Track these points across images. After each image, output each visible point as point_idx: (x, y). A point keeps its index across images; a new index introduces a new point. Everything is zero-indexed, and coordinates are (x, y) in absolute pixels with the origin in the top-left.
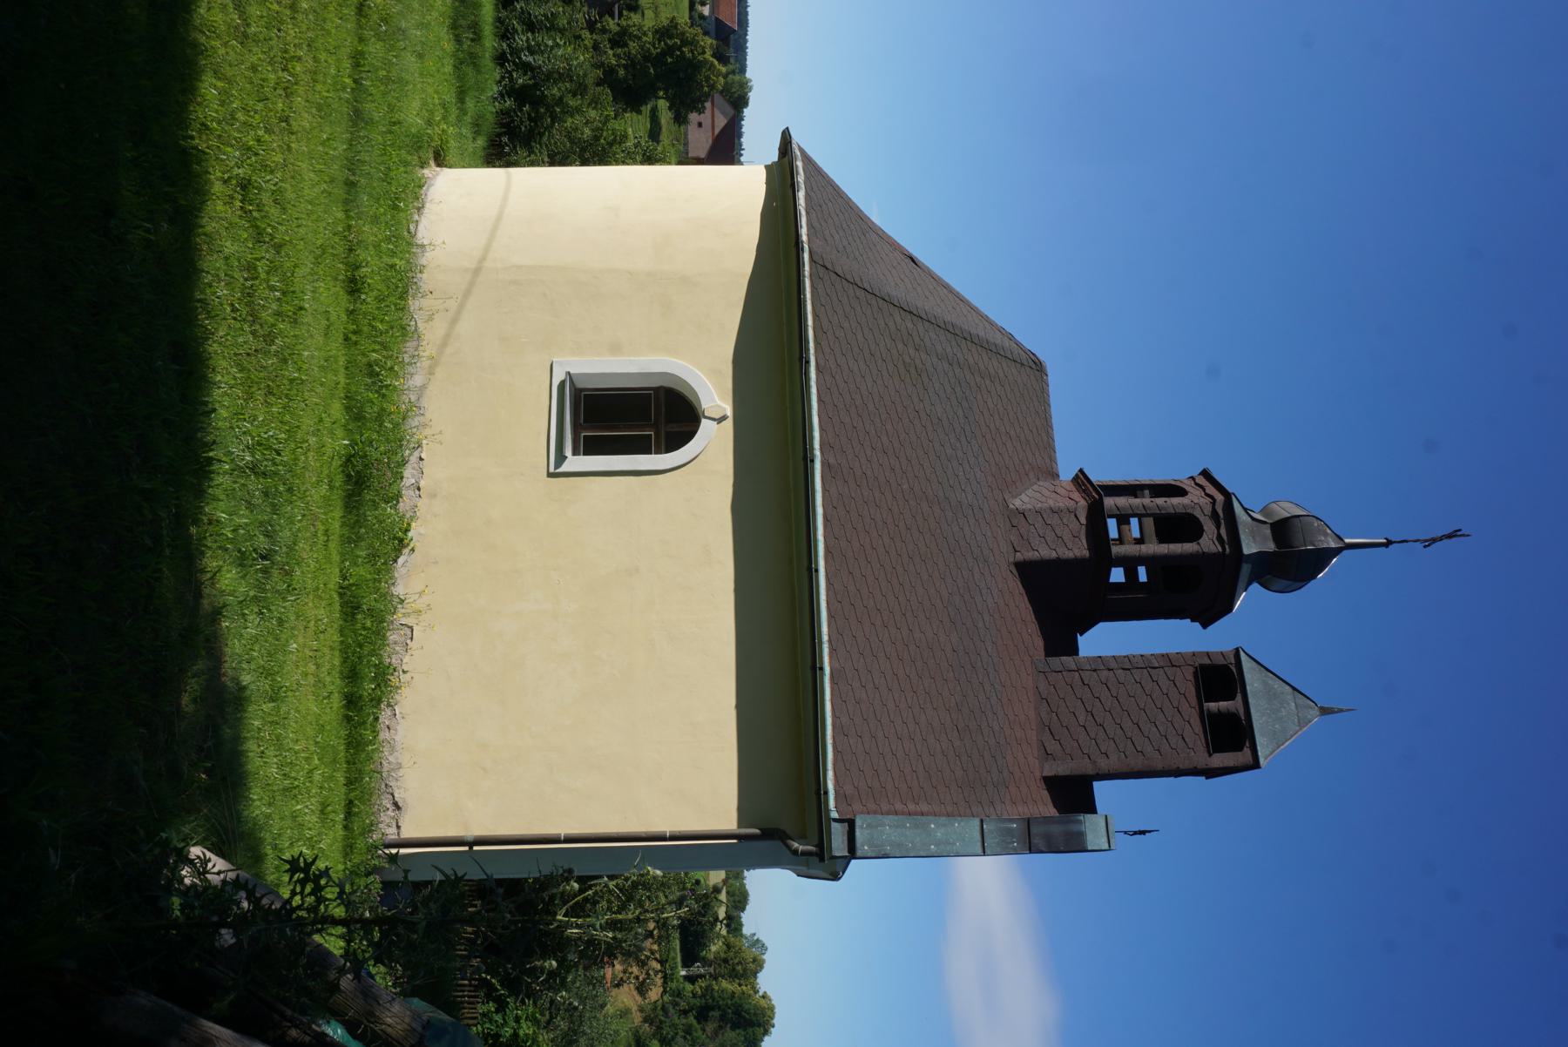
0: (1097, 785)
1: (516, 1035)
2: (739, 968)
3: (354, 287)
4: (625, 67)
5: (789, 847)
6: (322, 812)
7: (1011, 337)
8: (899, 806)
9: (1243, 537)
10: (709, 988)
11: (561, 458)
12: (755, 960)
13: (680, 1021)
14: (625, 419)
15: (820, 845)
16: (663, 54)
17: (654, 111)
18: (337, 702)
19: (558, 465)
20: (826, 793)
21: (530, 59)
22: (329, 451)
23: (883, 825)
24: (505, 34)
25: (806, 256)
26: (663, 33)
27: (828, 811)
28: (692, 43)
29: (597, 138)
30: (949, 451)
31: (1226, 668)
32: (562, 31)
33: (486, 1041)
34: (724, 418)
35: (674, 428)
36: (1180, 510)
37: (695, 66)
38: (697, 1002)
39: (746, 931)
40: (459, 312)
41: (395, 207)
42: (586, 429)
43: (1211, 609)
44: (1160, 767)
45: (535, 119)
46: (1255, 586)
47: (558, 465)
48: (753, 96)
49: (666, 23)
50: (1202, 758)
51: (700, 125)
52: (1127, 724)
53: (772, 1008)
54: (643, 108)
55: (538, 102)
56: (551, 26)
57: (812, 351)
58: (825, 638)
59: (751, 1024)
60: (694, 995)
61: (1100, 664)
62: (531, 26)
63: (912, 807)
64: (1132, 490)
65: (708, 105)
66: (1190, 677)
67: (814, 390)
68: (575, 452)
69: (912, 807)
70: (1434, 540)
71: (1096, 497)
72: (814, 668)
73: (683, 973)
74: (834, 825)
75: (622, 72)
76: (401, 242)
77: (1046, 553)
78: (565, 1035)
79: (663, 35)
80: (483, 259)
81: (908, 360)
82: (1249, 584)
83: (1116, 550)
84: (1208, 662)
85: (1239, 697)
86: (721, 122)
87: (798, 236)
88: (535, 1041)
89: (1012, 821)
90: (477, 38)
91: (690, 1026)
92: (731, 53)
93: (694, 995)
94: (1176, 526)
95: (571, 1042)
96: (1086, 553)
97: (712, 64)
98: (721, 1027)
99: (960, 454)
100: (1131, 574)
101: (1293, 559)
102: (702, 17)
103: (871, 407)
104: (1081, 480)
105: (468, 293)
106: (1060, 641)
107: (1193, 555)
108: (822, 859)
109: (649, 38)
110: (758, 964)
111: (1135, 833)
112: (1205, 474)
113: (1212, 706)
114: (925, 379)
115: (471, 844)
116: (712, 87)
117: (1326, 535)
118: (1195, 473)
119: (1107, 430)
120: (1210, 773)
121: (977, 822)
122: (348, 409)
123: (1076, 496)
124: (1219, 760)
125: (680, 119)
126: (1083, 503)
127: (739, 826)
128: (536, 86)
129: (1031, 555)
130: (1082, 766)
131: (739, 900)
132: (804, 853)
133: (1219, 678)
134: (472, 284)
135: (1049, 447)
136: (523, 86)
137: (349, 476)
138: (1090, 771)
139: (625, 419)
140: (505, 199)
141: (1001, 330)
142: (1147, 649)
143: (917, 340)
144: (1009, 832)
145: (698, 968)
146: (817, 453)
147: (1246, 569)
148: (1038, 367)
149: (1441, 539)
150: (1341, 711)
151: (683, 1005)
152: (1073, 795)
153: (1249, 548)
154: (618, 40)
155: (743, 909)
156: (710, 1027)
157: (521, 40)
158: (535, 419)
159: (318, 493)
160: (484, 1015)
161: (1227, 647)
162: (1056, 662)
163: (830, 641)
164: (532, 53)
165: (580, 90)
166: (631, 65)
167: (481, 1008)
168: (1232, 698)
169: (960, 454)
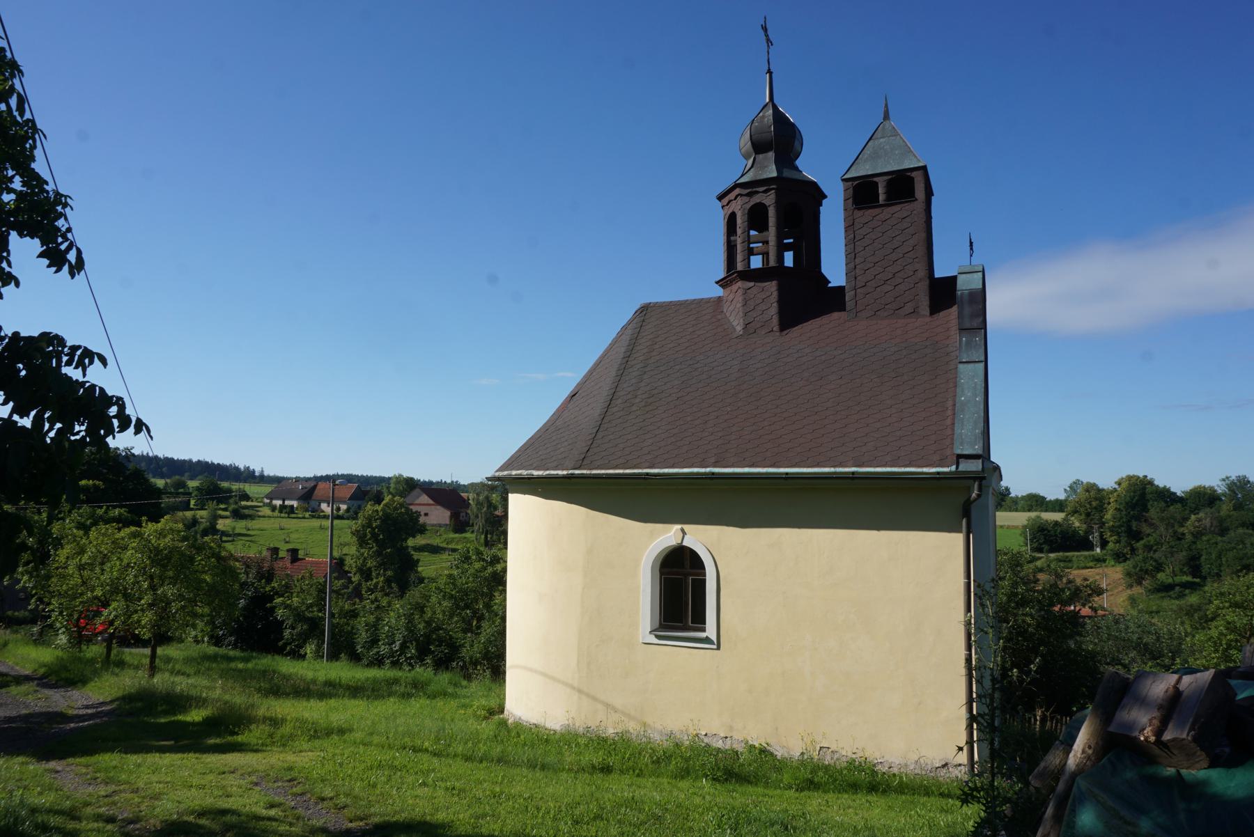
0: (938, 274)
2: (1094, 504)
3: (606, 770)
4: (385, 570)
5: (975, 500)
6: (947, 812)
7: (624, 328)
8: (949, 422)
9: (765, 176)
11: (707, 640)
12: (1087, 491)
14: (681, 596)
15: (975, 479)
16: (376, 541)
17: (421, 549)
18: (873, 798)
20: (938, 473)
22: (712, 791)
24: (378, 662)
26: (362, 542)
27: (950, 473)
28: (370, 519)
29: (452, 597)
31: (855, 188)
32: (378, 619)
34: (682, 530)
35: (687, 563)
36: (746, 217)
37: (386, 518)
38: (1124, 539)
39: (1062, 497)
40: (607, 705)
41: (547, 741)
43: (815, 194)
44: (924, 235)
45: (441, 641)
46: (798, 163)
48: (407, 474)
49: (355, 539)
50: (919, 205)
51: (426, 514)
53: (1130, 478)
54: (415, 557)
55: (428, 639)
56: (374, 627)
58: (832, 470)
59: (1143, 495)
60: (1118, 542)
61: (851, 273)
62: (374, 642)
63: (949, 412)
65: (414, 508)
66: (861, 213)
67: (666, 471)
68: (704, 630)
69: (949, 412)
70: (768, 40)
71: (734, 274)
72: (853, 478)
73: (1098, 550)
74: (961, 468)
75: (389, 573)
76: (568, 739)
77: (774, 310)
80: (573, 688)
82: (796, 169)
83: (772, 263)
85: (876, 179)
86: (425, 499)
87: (564, 477)
89: (961, 340)
90: (396, 681)
93: (1118, 542)
94: (757, 218)
96: (774, 283)
97: (386, 505)
100: (788, 247)
101: (779, 139)
102: (348, 510)
104: (723, 283)
105: (595, 699)
106: (833, 300)
107: (775, 209)
108: (984, 478)
109: (365, 552)
110: (1091, 488)
112: (720, 198)
113: (882, 198)
114: (655, 392)
116: (402, 505)
118: (719, 204)
119: (690, 266)
120: (929, 193)
121: (961, 366)
122: (682, 778)
123: (735, 287)
124: (920, 192)
125: (422, 530)
126: (740, 284)
127: (960, 532)
128: (417, 640)
130: (924, 287)
131: (1035, 502)
132: (980, 489)
133: (862, 192)
134: (588, 695)
135: (700, 303)
136: (417, 649)
137: (726, 780)
138: (927, 282)
139: (681, 596)
140: (531, 670)
141: (620, 335)
142: (842, 242)
144: (968, 343)
145: (1095, 538)
146: (708, 470)
147: (787, 173)
148: (645, 310)
149: (767, 36)
150: (886, 106)
152: (943, 293)
154: (366, 574)
155: (1044, 498)
156: (1146, 529)
157: (384, 649)
158: (679, 657)
159: (742, 797)
161: (841, 186)
163: (834, 466)
165: (421, 609)
166: (382, 565)
168: (877, 184)
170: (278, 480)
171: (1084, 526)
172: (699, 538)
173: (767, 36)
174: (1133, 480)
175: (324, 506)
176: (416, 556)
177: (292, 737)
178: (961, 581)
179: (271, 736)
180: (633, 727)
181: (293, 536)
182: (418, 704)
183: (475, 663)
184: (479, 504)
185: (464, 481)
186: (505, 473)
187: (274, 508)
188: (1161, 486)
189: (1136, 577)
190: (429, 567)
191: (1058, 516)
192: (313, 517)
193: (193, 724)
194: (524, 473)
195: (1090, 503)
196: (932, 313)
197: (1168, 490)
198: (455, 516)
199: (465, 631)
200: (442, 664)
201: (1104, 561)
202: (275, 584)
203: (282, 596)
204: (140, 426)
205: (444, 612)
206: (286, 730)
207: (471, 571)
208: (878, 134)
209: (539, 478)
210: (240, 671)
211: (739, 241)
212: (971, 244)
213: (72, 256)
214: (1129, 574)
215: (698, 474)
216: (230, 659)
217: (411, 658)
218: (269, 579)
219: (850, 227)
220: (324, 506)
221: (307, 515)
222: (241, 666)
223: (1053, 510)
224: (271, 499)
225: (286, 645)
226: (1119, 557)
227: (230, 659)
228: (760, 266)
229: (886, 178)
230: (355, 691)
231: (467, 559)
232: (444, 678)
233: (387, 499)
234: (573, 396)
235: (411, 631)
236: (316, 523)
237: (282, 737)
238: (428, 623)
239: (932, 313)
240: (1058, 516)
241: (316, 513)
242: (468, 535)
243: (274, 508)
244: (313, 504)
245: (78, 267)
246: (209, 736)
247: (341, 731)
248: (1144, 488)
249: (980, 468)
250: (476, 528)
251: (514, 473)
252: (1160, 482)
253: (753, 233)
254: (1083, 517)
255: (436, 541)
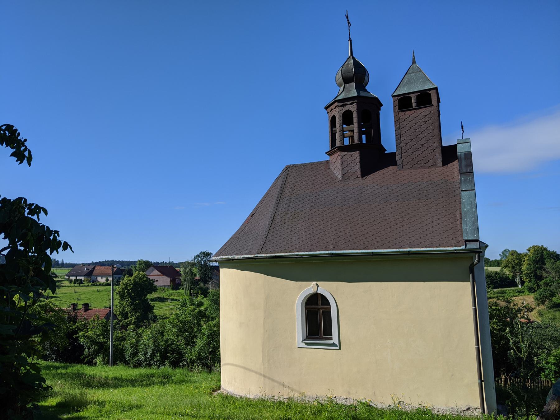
1: (554, 364)
2: (516, 261)
4: (136, 313)
5: (477, 264)
7: (278, 179)
8: (458, 222)
9: (351, 96)
10: (526, 275)
11: (334, 345)
13: (543, 288)
14: (318, 322)
15: (476, 253)
16: (130, 297)
17: (152, 300)
19: (336, 346)
21: (149, 353)
23: (466, 229)
24: (138, 365)
25: (259, 255)
26: (122, 297)
27: (462, 250)
28: (126, 285)
30: (323, 202)
32: (138, 341)
33: (558, 377)
34: (317, 284)
37: (136, 284)
38: (533, 280)
39: (499, 258)
42: (321, 335)
43: (376, 104)
46: (366, 88)
47: (336, 346)
48: (145, 259)
51: (157, 281)
52: (422, 136)
53: (534, 247)
54: (152, 305)
55: (166, 349)
56: (135, 346)
57: (293, 254)
58: (397, 250)
59: (542, 256)
60: (530, 281)
62: (136, 353)
64: (333, 135)
69: (458, 217)
70: (349, 23)
71: (334, 148)
73: (520, 286)
75: (138, 314)
77: (358, 166)
78: (553, 342)
79: (123, 297)
80: (261, 374)
81: (291, 218)
82: (366, 91)
84: (397, 107)
86: (156, 272)
87: (252, 258)
88: (556, 356)
90: (153, 375)
91: (544, 283)
92: (127, 268)
93: (530, 281)
94: (347, 118)
95: (556, 340)
96: (358, 152)
97: (135, 277)
98: (544, 270)
99: (323, 198)
100: (364, 133)
101: (357, 75)
103: (310, 232)
104: (330, 153)
105: (273, 380)
106: (390, 160)
110: (514, 253)
111: (463, 130)
113: (414, 105)
114: (297, 211)
115: (482, 381)
116: (144, 276)
117: (348, 64)
118: (326, 111)
119: (312, 143)
121: (462, 193)
123: (336, 155)
125: (155, 289)
126: (339, 153)
129: (359, 172)
132: (479, 258)
133: (403, 103)
134: (269, 378)
136: (160, 356)
139: (318, 322)
140: (236, 365)
143: (283, 214)
145: (517, 280)
146: (330, 252)
147: (362, 94)
148: (288, 168)
149: (348, 21)
150: (414, 56)
151: (535, 286)
152: (449, 154)
153: (354, 93)
156: (545, 274)
157: (142, 357)
158: (318, 354)
160: (546, 377)
162: (398, 162)
163: (398, 248)
164: (147, 353)
165: (162, 334)
166: (135, 310)
167: (543, 378)
169: (323, 198)
170: (72, 266)
171: (512, 274)
172: (326, 288)
173: (348, 21)
174: (536, 248)
175: (99, 279)
176: (152, 304)
177: (111, 412)
178: (471, 308)
179: (100, 411)
180: (296, 396)
181: (82, 296)
182: (170, 388)
183: (193, 362)
184: (186, 273)
185: (176, 261)
186: (219, 257)
187: (71, 281)
188: (551, 251)
189: (541, 300)
190: (159, 309)
191: (497, 269)
192: (93, 285)
193: (52, 407)
194: (230, 257)
195: (514, 261)
196: (444, 165)
197: (555, 253)
198: (173, 281)
199: (186, 344)
200: (175, 364)
201: (523, 292)
202: (78, 324)
203: (82, 331)
204: (66, 246)
205: (173, 334)
206: (108, 407)
207: (188, 311)
208: (410, 71)
209: (238, 259)
210: (64, 374)
211: (338, 131)
212: (462, 127)
213: (26, 153)
214: (537, 299)
215: (324, 254)
216: (57, 368)
217: (157, 361)
218: (75, 322)
219: (397, 121)
220: (99, 279)
221: (90, 284)
222: (64, 371)
223: (494, 266)
224: (69, 276)
225: (84, 358)
226: (531, 290)
227: (57, 368)
228: (348, 144)
229: (416, 94)
230: (132, 382)
231: (184, 304)
232: (178, 373)
233: (135, 274)
234: (252, 215)
235: (156, 346)
236: (95, 288)
237: (106, 412)
238: (166, 341)
239: (444, 165)
240: (497, 269)
241: (95, 283)
242: (180, 291)
243: (71, 281)
244: (93, 278)
245: (30, 159)
246: (64, 413)
247: (138, 407)
248: (543, 252)
249: (478, 247)
250: (185, 287)
251: (224, 257)
252: (551, 249)
253: (344, 126)
254: (511, 269)
255: (163, 295)
